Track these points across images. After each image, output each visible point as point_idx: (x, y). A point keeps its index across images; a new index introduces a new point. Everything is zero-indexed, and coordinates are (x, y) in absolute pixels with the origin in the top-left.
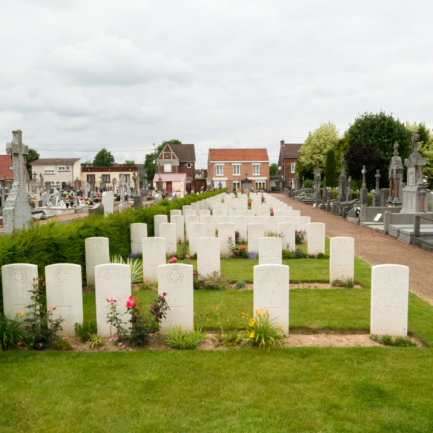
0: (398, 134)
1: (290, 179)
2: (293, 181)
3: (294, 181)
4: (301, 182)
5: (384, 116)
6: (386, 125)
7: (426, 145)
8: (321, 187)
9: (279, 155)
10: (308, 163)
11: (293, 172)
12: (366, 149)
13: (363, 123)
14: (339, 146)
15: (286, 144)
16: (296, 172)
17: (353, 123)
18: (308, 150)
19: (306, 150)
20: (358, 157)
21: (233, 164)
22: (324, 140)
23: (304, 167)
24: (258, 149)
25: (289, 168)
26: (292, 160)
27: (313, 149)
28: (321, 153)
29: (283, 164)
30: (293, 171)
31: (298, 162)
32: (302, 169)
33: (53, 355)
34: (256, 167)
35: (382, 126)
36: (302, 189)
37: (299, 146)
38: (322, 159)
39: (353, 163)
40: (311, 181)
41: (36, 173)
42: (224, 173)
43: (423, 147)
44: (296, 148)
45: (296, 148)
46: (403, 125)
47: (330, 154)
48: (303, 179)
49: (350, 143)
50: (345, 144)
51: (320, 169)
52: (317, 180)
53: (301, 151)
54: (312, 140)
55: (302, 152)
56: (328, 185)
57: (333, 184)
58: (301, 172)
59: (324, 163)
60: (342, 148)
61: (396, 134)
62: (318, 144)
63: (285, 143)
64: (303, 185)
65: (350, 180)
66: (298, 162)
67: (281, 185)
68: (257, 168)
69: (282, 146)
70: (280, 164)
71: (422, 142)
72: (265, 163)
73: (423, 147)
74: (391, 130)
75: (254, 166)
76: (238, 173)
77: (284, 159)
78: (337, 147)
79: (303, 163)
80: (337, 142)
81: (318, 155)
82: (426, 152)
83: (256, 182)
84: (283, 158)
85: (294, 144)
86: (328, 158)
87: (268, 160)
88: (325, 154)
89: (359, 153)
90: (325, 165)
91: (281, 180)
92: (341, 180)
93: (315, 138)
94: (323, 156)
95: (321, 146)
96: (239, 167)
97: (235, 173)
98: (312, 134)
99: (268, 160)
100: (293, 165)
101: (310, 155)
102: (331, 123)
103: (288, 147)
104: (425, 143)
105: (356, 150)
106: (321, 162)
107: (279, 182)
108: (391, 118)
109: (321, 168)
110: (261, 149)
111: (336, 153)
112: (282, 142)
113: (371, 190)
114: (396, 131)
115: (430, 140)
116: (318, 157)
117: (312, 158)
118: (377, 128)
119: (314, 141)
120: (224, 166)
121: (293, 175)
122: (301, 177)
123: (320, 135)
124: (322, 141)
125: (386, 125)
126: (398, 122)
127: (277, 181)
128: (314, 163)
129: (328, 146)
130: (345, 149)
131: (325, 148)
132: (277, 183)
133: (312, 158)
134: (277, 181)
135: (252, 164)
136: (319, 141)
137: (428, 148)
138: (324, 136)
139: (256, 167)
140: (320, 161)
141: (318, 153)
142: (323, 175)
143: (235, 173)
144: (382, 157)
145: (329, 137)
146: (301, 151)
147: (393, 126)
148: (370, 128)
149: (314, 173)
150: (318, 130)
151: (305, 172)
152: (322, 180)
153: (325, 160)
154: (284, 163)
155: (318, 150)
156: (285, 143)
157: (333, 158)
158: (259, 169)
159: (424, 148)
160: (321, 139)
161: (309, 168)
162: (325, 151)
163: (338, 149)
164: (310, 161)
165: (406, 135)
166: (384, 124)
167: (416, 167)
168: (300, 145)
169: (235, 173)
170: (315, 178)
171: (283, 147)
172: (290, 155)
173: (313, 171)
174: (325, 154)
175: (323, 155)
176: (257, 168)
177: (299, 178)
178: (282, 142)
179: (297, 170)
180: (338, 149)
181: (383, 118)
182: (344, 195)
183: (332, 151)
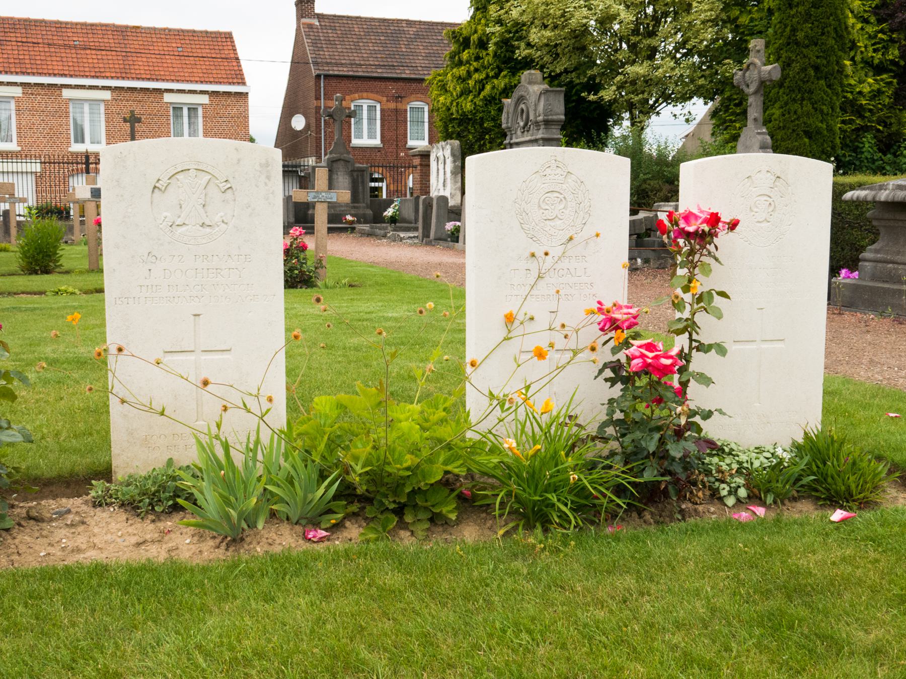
15: (320, 17)
21: (168, 98)
24: (193, 33)
26: (351, 85)
29: (315, 103)
33: (646, 82)
34: (185, 112)
41: (128, 116)
42: (19, 136)
44: (367, 34)
45: (367, 34)
65: (693, 241)
69: (304, 20)
72: (228, 94)
75: (178, 109)
76: (371, 136)
77: (318, 77)
84: (314, 73)
87: (244, 84)
96: (200, 112)
97: (359, 136)
120: (17, 100)
135: (168, 98)
139: (185, 112)
143: (83, 141)
154: (318, 98)
158: (200, 120)
169: (83, 141)
171: (310, 26)
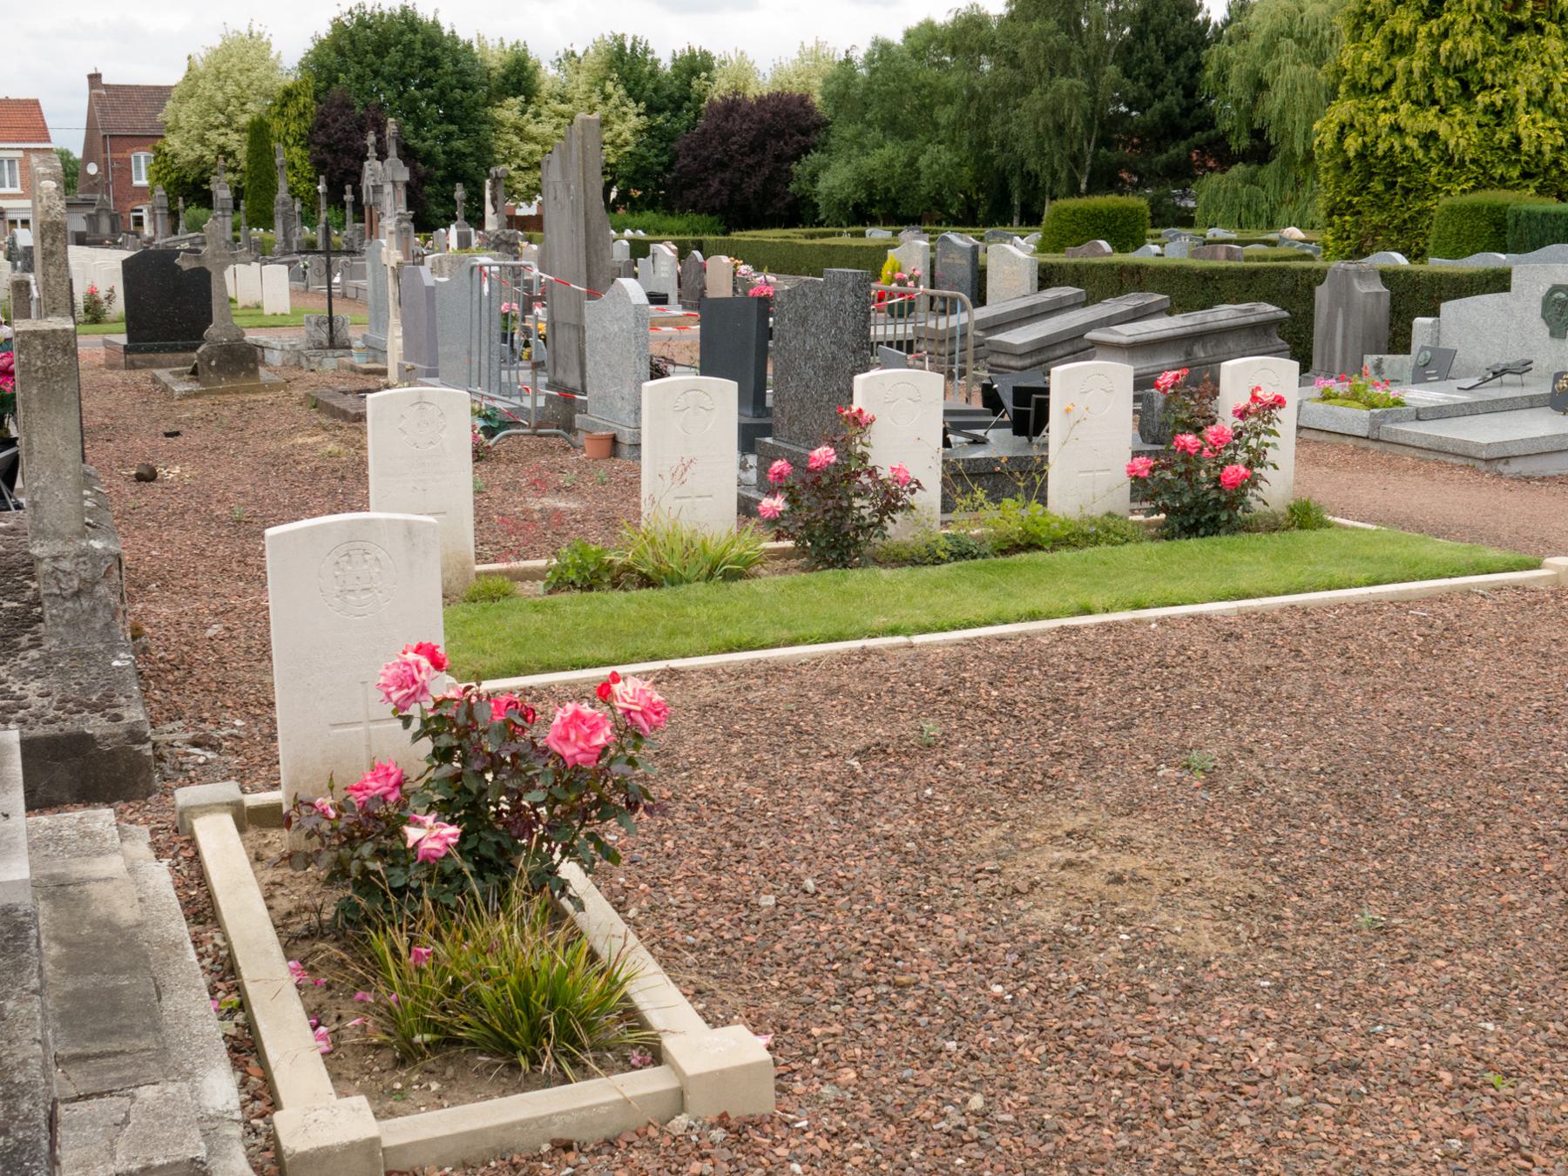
0: (453, 73)
1: (130, 207)
2: (145, 215)
3: (152, 212)
4: (174, 215)
5: (414, 18)
6: (418, 45)
7: (532, 109)
8: (236, 228)
9: (84, 125)
10: (193, 156)
11: (141, 181)
12: (363, 117)
13: (351, 34)
14: (285, 105)
15: (107, 87)
16: (153, 185)
17: (324, 30)
18: (187, 114)
19: (182, 116)
20: (340, 140)
22: (239, 86)
23: (180, 169)
25: (125, 170)
26: (136, 141)
27: (203, 114)
28: (228, 125)
30: (139, 178)
31: (158, 151)
32: (174, 175)
34: (6, 164)
35: (408, 51)
36: (179, 237)
37: (159, 94)
38: (235, 146)
39: (328, 158)
40: (205, 210)
43: (523, 112)
46: (470, 46)
47: (259, 133)
48: (181, 205)
49: (316, 97)
50: (302, 100)
51: (230, 176)
52: (223, 209)
53: (166, 115)
54: (201, 83)
55: (170, 119)
56: (253, 222)
57: (266, 221)
58: (170, 184)
59: (241, 155)
60: (292, 111)
61: (446, 74)
62: (219, 97)
63: (105, 81)
64: (181, 223)
66: (158, 151)
67: (105, 225)
68: (11, 169)
70: (89, 155)
71: (522, 98)
73: (523, 112)
74: (434, 63)
78: (277, 109)
79: (175, 156)
80: (278, 94)
81: (222, 130)
82: (532, 128)
83: (10, 216)
84: (102, 133)
85: (137, 87)
86: (251, 143)
88: (243, 130)
89: (344, 130)
90: (244, 164)
91: (103, 209)
92: (278, 209)
93: (210, 77)
94: (236, 137)
95: (228, 103)
98: (199, 63)
99: (49, 141)
100: (138, 158)
101: (194, 132)
102: (256, 29)
103: (117, 96)
104: (528, 102)
105: (335, 120)
106: (232, 154)
107: (97, 215)
108: (436, 25)
109: (234, 170)
110: (19, 101)
111: (277, 127)
112: (94, 79)
113: (702, 322)
114: (448, 66)
115: (544, 94)
116: (222, 140)
117: (202, 141)
118: (394, 55)
119: (207, 87)
121: (143, 193)
122: (172, 200)
123: (224, 68)
124: (230, 88)
125: (418, 45)
126: (453, 37)
127: (92, 211)
128: (210, 157)
129: (250, 106)
130: (301, 115)
131: (244, 112)
132: (92, 220)
133: (202, 141)
134: (92, 211)
136: (221, 88)
137: (537, 115)
138: (236, 75)
140: (229, 149)
141: (223, 125)
142: (238, 193)
144: (411, 142)
145: (254, 75)
146: (166, 115)
147: (437, 51)
148: (375, 53)
149: (212, 187)
150: (216, 52)
151: (184, 183)
152: (236, 207)
153: (245, 148)
155: (222, 118)
156: (105, 81)
157: (268, 142)
159: (527, 116)
160: (230, 81)
161: (197, 170)
162: (243, 120)
163: (281, 114)
164: (199, 150)
165: (477, 79)
166: (411, 42)
167: (394, 183)
168: (169, 88)
170: (217, 204)
171: (99, 96)
172: (126, 123)
173: (207, 182)
174: (243, 130)
175: (237, 131)
176: (11, 169)
177: (165, 203)
178: (94, 79)
179: (157, 176)
180: (281, 114)
181: (409, 22)
182: (288, 242)
183: (261, 120)
